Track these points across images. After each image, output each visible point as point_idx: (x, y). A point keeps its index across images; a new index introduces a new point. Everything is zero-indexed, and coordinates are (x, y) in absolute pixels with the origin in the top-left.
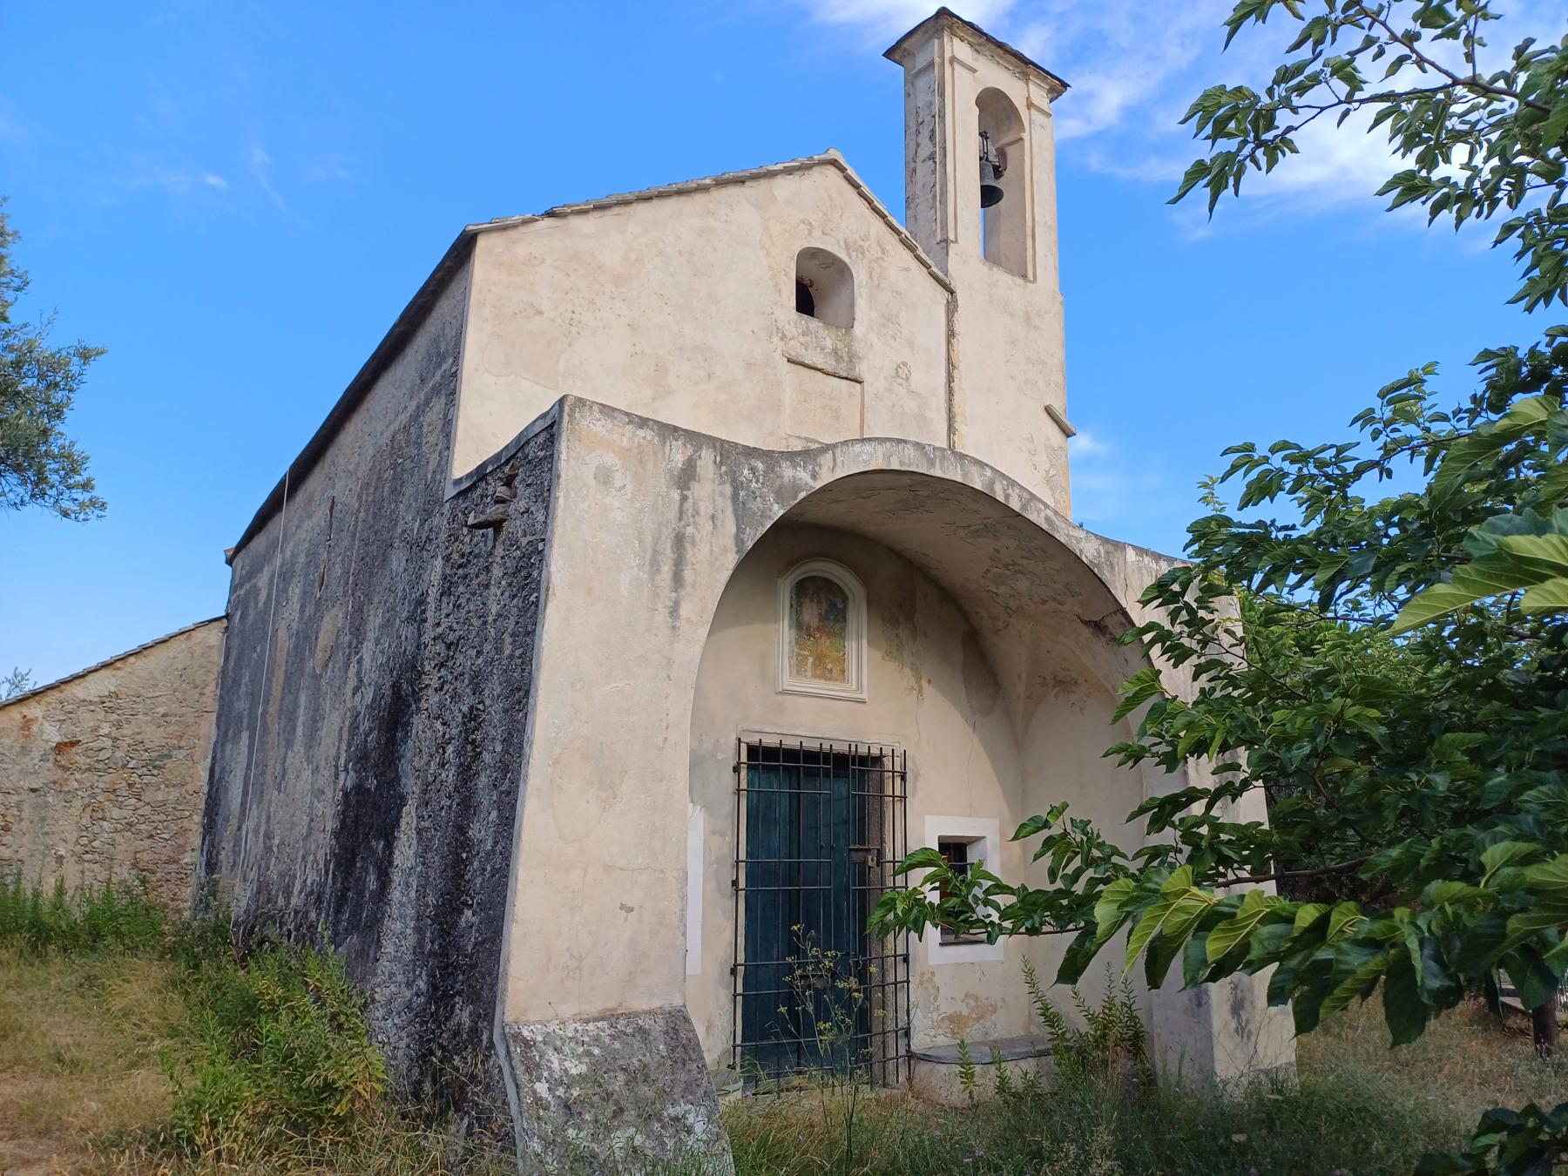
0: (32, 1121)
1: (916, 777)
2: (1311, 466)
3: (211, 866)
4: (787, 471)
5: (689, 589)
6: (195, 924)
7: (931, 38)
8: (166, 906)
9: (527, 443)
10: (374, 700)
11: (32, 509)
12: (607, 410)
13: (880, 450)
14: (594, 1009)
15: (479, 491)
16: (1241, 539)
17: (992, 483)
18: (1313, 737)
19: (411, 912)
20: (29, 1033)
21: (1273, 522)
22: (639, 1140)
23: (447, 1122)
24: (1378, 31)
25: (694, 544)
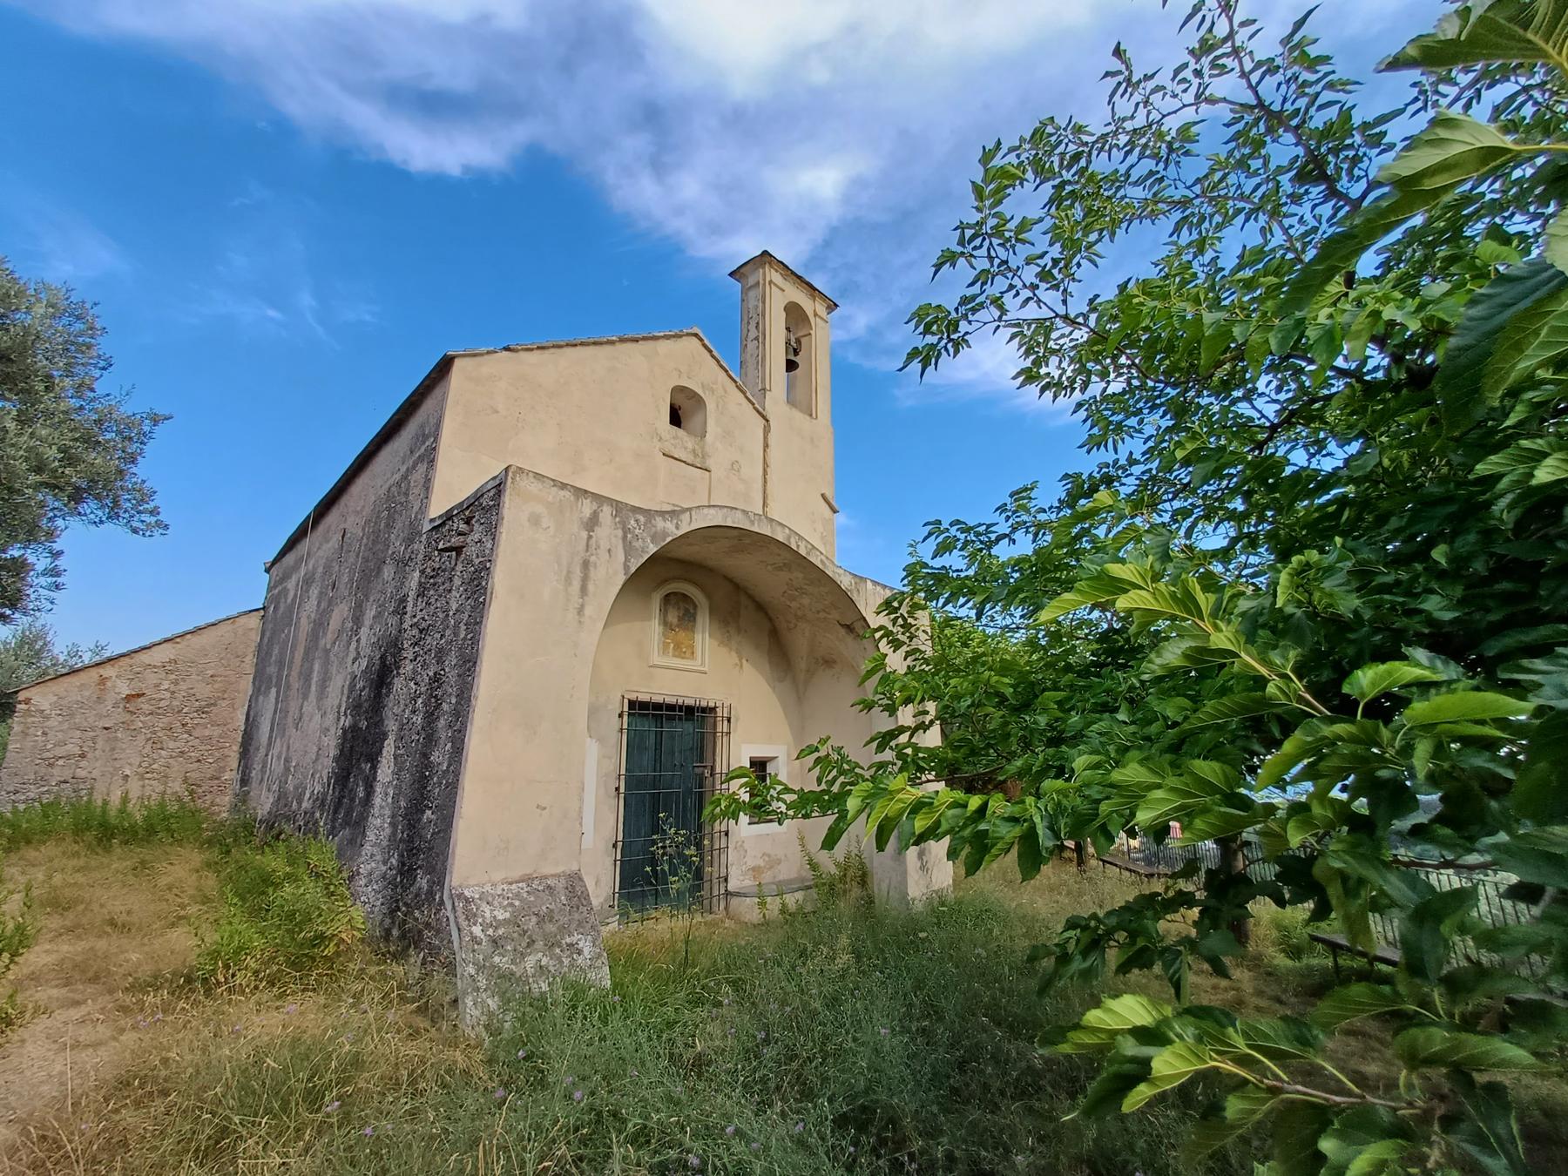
3: (245, 781)
4: (660, 523)
11: (108, 527)
13: (721, 513)
14: (516, 875)
17: (789, 538)
19: (387, 812)
24: (1016, 281)
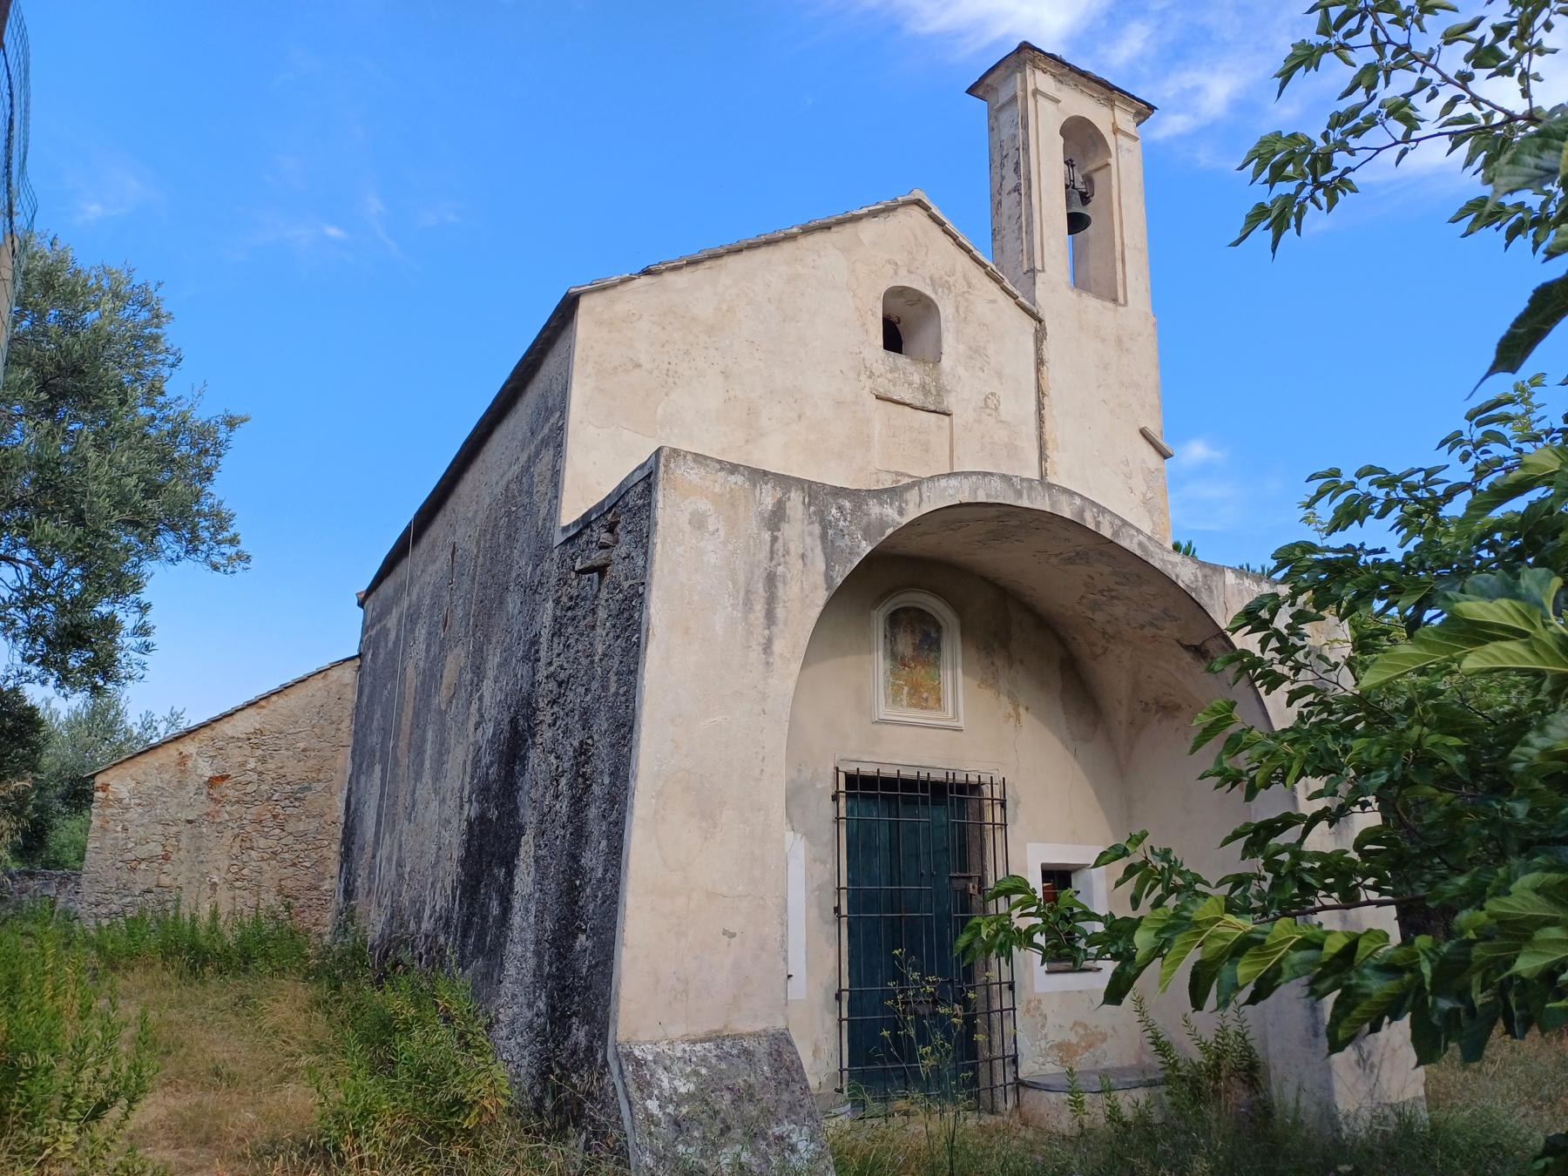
0: (193, 1132)
1: (1017, 804)
2: (1399, 489)
3: (349, 893)
4: (874, 509)
5: (781, 626)
6: (335, 948)
7: (1013, 72)
8: (309, 930)
9: (627, 492)
10: (494, 735)
11: (187, 564)
12: (700, 459)
13: (966, 483)
14: (700, 1030)
15: (585, 537)
16: (1327, 565)
17: (1081, 512)
18: (1390, 766)
19: (530, 936)
20: (190, 1049)
21: (1362, 545)
22: (745, 1156)
23: (567, 1137)
24: (1429, 74)
25: (784, 582)
